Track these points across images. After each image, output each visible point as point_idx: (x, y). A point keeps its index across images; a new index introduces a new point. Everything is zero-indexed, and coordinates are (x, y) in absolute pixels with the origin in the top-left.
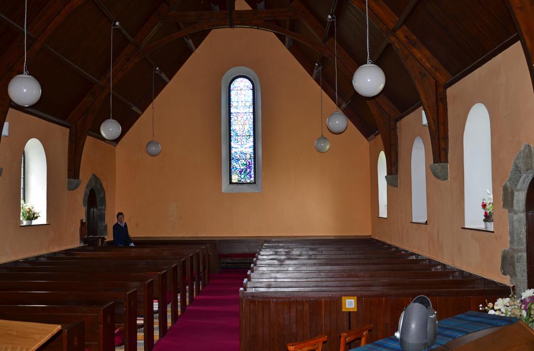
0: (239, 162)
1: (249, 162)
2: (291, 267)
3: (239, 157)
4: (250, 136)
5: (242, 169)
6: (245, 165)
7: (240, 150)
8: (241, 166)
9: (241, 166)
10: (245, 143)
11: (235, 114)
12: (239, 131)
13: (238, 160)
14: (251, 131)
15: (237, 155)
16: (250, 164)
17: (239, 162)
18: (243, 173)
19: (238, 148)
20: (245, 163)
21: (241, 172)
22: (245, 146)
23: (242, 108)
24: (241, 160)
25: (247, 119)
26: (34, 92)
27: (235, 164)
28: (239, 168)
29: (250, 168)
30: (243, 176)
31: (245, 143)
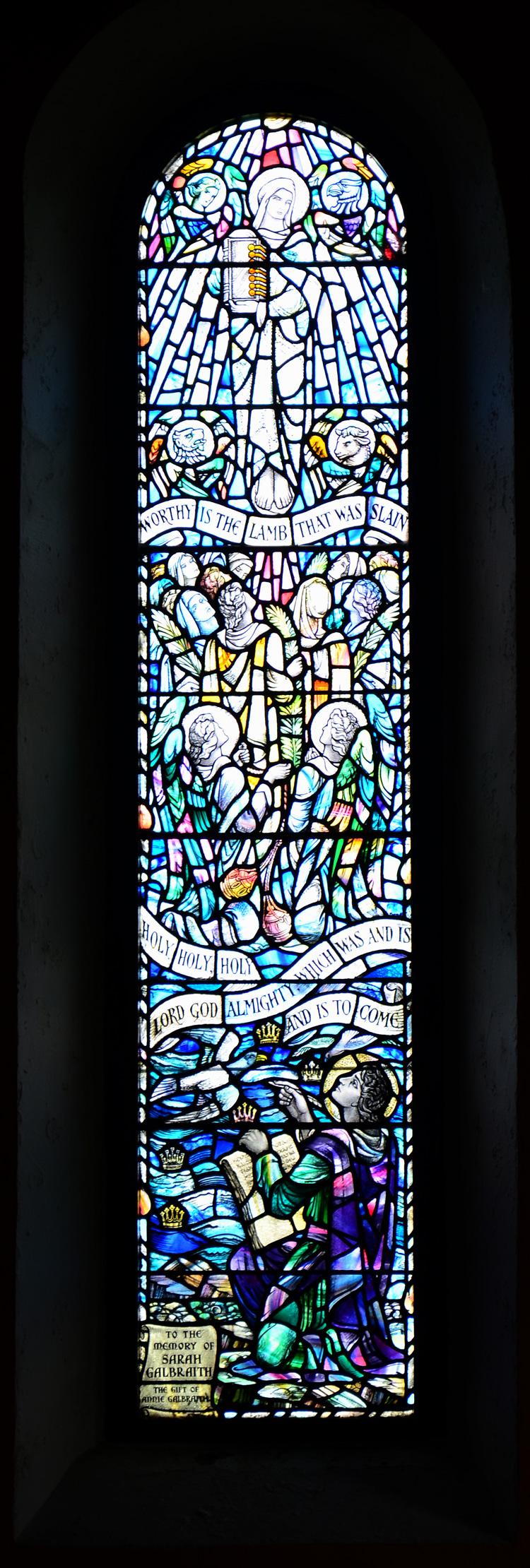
0: (238, 1162)
1: (359, 1166)
2: (298, 823)
3: (230, 1097)
4: (368, 834)
5: (277, 1252)
6: (303, 1194)
7: (250, 1007)
8: (256, 1206)
9: (256, 1206)
10: (310, 921)
11: (185, 568)
12: (233, 780)
13: (225, 1133)
14: (387, 780)
15: (213, 1078)
16: (365, 1188)
17: (238, 1162)
18: (276, 1295)
19: (219, 987)
20: (307, 1173)
21: (250, 1295)
22: (318, 962)
23: (272, 491)
24: (256, 1140)
25: (334, 623)
26: (279, 199)
27: (176, 1185)
28: (228, 1228)
29: (372, 1235)
30: (275, 1340)
31: (310, 921)
